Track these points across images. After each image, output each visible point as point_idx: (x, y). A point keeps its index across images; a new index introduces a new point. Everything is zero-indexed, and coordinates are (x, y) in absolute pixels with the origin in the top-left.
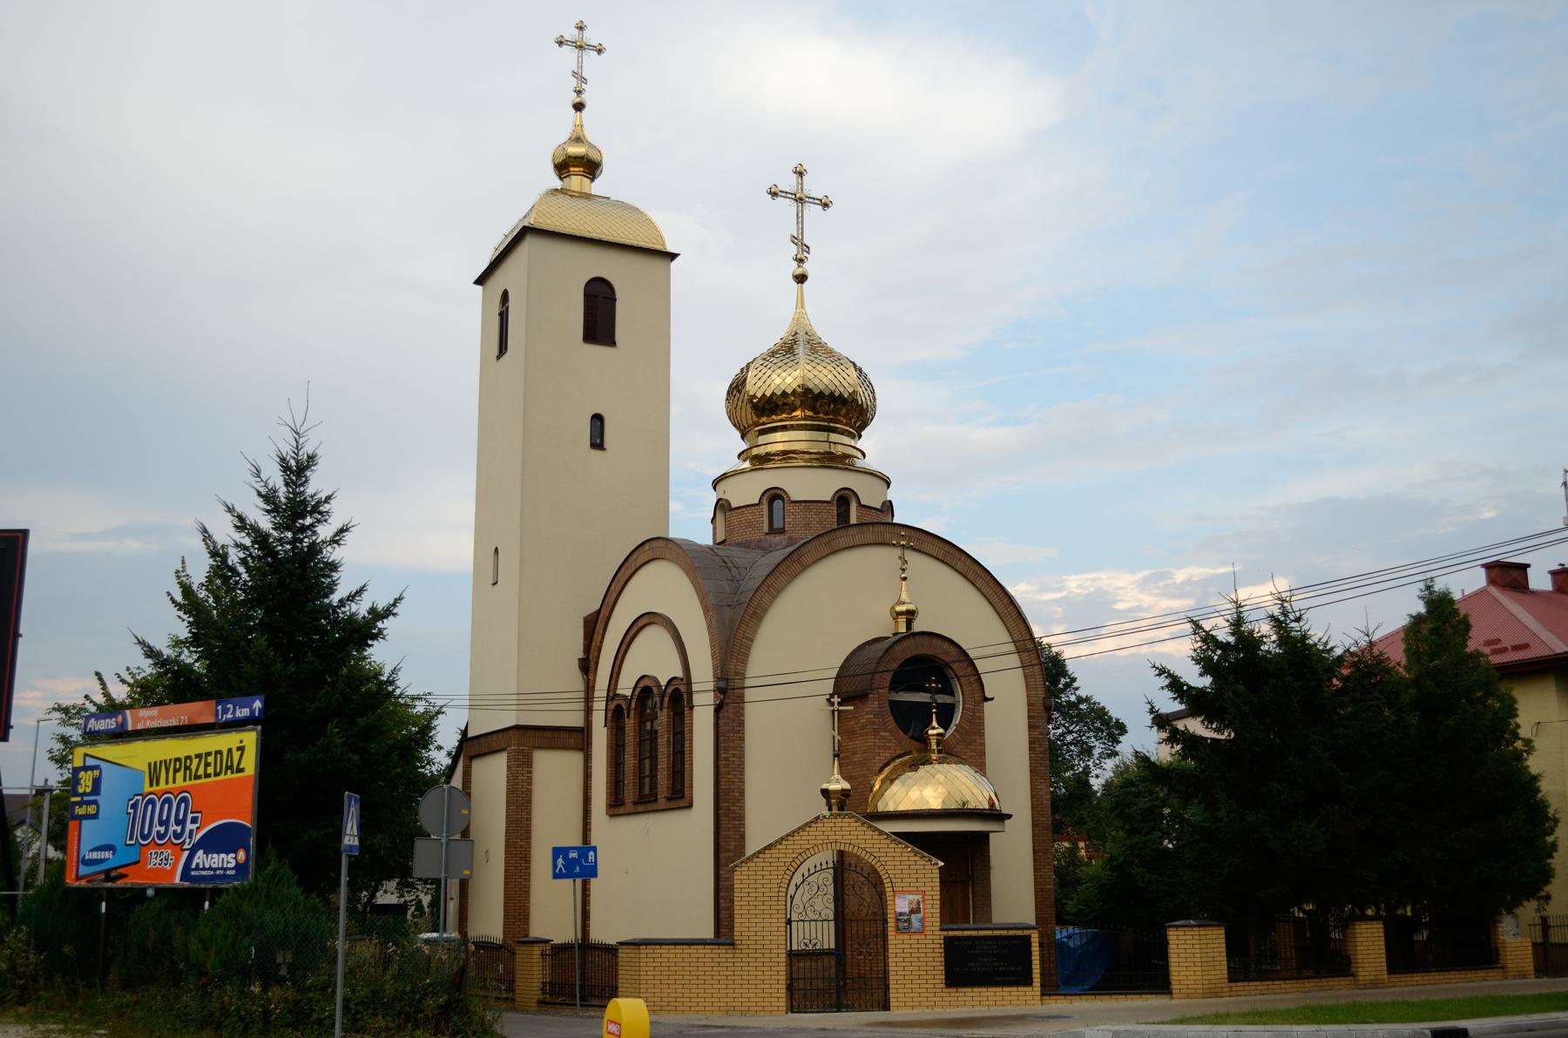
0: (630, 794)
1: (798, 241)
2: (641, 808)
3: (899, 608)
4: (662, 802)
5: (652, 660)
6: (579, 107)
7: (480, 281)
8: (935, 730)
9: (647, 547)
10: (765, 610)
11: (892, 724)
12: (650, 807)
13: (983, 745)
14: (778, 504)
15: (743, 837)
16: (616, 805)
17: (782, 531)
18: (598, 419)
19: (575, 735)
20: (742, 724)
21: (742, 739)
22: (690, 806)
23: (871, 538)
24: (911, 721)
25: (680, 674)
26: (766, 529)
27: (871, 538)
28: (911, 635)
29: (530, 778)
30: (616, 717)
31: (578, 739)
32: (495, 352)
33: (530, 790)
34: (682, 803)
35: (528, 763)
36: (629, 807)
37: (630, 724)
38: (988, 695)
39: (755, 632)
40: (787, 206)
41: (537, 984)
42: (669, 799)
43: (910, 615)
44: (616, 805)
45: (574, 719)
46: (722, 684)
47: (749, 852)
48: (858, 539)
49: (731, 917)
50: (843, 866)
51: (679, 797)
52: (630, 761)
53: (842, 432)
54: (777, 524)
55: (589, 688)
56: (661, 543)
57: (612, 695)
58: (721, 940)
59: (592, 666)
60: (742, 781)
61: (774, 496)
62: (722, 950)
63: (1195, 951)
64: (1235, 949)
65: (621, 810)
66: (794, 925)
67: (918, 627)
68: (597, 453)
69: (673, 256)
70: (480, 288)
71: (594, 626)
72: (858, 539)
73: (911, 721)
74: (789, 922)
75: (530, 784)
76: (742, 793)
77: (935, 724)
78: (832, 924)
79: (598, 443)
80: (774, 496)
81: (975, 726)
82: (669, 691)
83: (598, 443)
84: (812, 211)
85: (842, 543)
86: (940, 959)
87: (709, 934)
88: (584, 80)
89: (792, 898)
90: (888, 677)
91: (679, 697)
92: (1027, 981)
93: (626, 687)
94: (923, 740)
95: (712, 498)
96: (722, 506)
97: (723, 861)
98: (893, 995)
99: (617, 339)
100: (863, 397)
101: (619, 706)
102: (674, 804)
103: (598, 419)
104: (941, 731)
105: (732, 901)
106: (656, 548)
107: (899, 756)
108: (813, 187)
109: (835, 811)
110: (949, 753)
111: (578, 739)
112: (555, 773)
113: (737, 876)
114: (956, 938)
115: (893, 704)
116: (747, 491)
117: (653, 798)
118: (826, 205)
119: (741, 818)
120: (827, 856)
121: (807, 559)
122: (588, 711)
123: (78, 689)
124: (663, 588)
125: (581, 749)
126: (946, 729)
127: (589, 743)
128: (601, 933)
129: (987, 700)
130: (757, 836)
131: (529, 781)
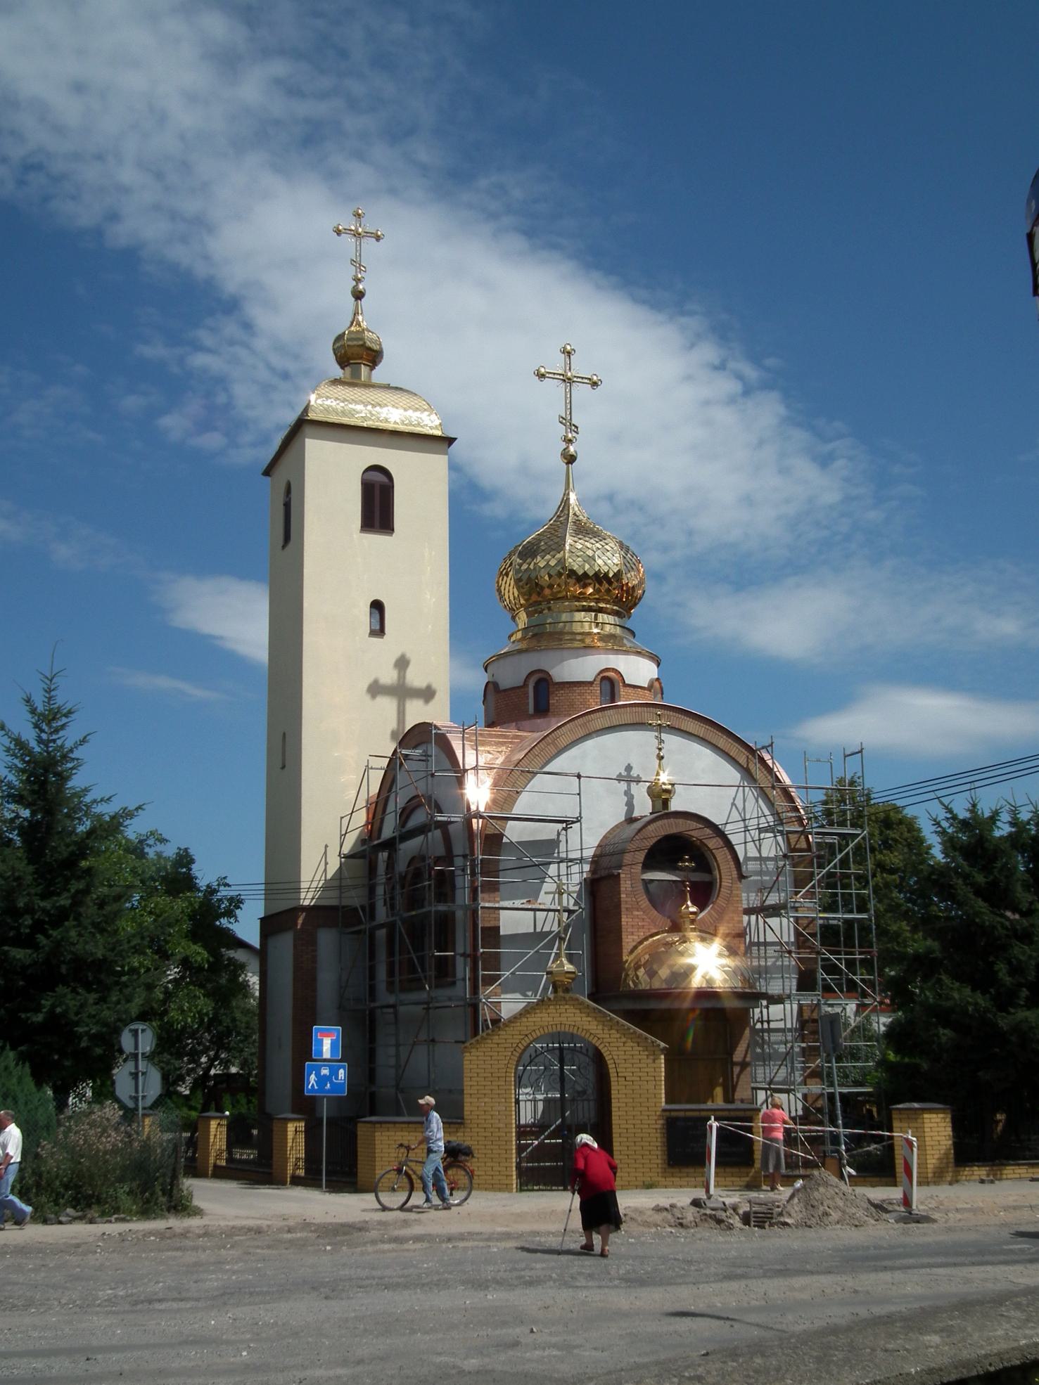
6: (358, 295)
7: (267, 472)
32: (281, 542)
40: (554, 389)
63: (929, 1133)
64: (960, 1128)
66: (522, 1104)
70: (269, 479)
84: (581, 391)
90: (641, 857)
95: (484, 678)
98: (925, 1188)
103: (377, 606)
108: (580, 368)
109: (561, 994)
115: (646, 883)
118: (595, 384)
122: (372, 890)
123: (95, 797)
126: (702, 910)
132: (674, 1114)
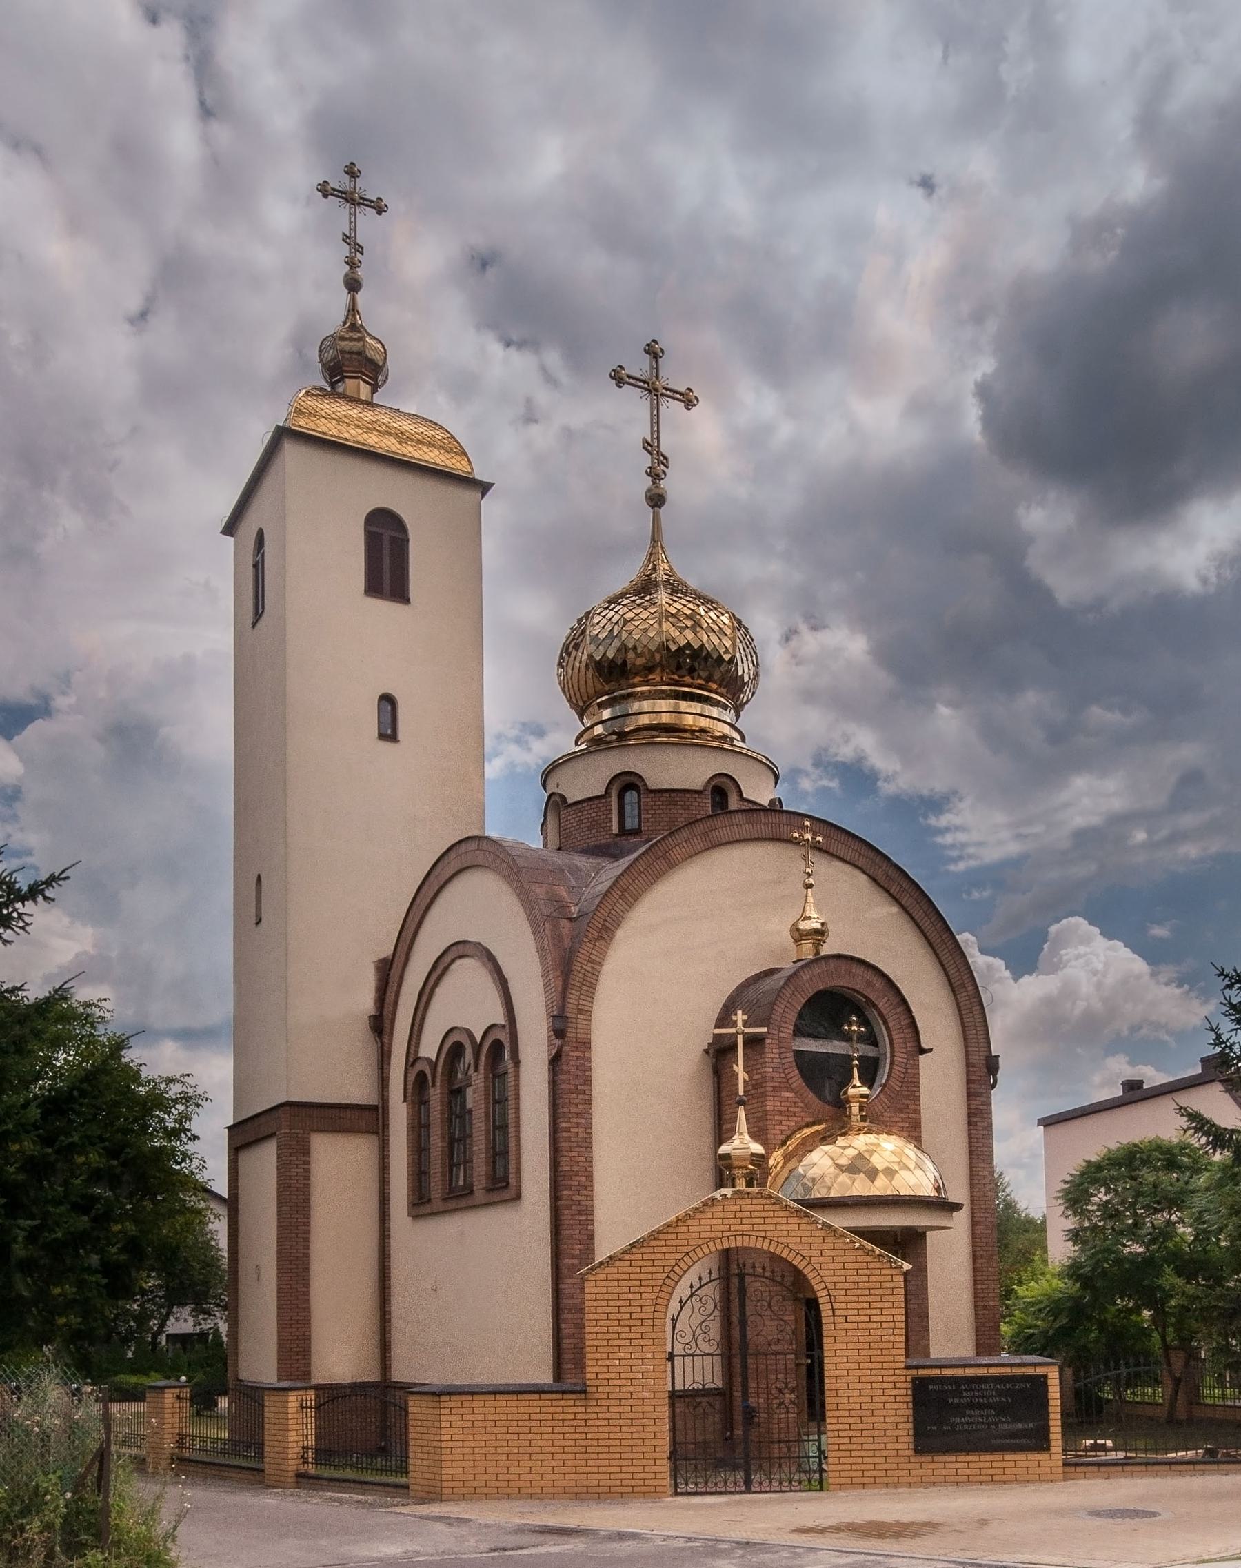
0: (436, 1188)
1: (651, 446)
2: (452, 1205)
3: (804, 925)
4: (479, 1195)
5: (466, 1005)
7: (230, 529)
8: (857, 1089)
9: (453, 854)
10: (618, 921)
11: (797, 1081)
12: (463, 1203)
13: (917, 1112)
14: (631, 796)
15: (591, 1237)
16: (421, 1204)
17: (637, 832)
18: (388, 700)
19: (366, 1114)
20: (588, 1081)
21: (589, 1102)
22: (518, 1197)
23: (763, 830)
24: (824, 1078)
25: (500, 1019)
26: (615, 830)
27: (763, 830)
28: (819, 959)
29: (307, 1171)
30: (418, 1087)
31: (367, 1119)
32: (250, 618)
33: (308, 1186)
34: (506, 1195)
35: (304, 1151)
36: (437, 1204)
37: (436, 1095)
38: (924, 1045)
39: (604, 955)
41: (294, 1450)
42: (489, 1190)
43: (819, 934)
44: (421, 1204)
45: (358, 1091)
46: (559, 1025)
47: (601, 1255)
48: (746, 830)
49: (390, 1052)
50: (733, 1271)
51: (502, 1186)
52: (437, 1142)
53: (716, 704)
54: (630, 824)
55: (384, 1057)
56: (473, 845)
57: (412, 1059)
58: (565, 1387)
59: (387, 1025)
60: (589, 1160)
61: (628, 783)
62: (569, 1400)
65: (427, 1209)
67: (825, 950)
68: (387, 746)
69: (484, 488)
71: (388, 974)
72: (746, 830)
73: (824, 1078)
74: (671, 1357)
75: (308, 1178)
76: (590, 1177)
77: (857, 1082)
78: (717, 1359)
79: (389, 733)
80: (628, 783)
81: (911, 1083)
82: (486, 1047)
83: (389, 733)
84: (672, 409)
85: (724, 834)
86: (906, 1410)
87: (545, 1376)
88: (360, 249)
89: (674, 1320)
91: (498, 1051)
92: (1040, 1442)
93: (429, 1048)
94: (841, 1104)
96: (556, 803)
97: (565, 1271)
99: (411, 596)
100: (744, 669)
101: (422, 1075)
102: (495, 1197)
103: (388, 700)
104: (865, 1090)
105: (582, 1326)
106: (466, 854)
107: (808, 1125)
110: (876, 1121)
111: (367, 1119)
112: (338, 1163)
113: (590, 1287)
114: (932, 1380)
115: (798, 1054)
116: (586, 782)
117: (469, 1191)
119: (588, 1211)
120: (700, 1270)
121: (676, 854)
124: (480, 908)
125: (377, 1133)
127: (385, 1126)
128: (401, 1373)
129: (923, 1051)
130: (607, 1244)
131: (307, 1173)
132: (923, 1373)
